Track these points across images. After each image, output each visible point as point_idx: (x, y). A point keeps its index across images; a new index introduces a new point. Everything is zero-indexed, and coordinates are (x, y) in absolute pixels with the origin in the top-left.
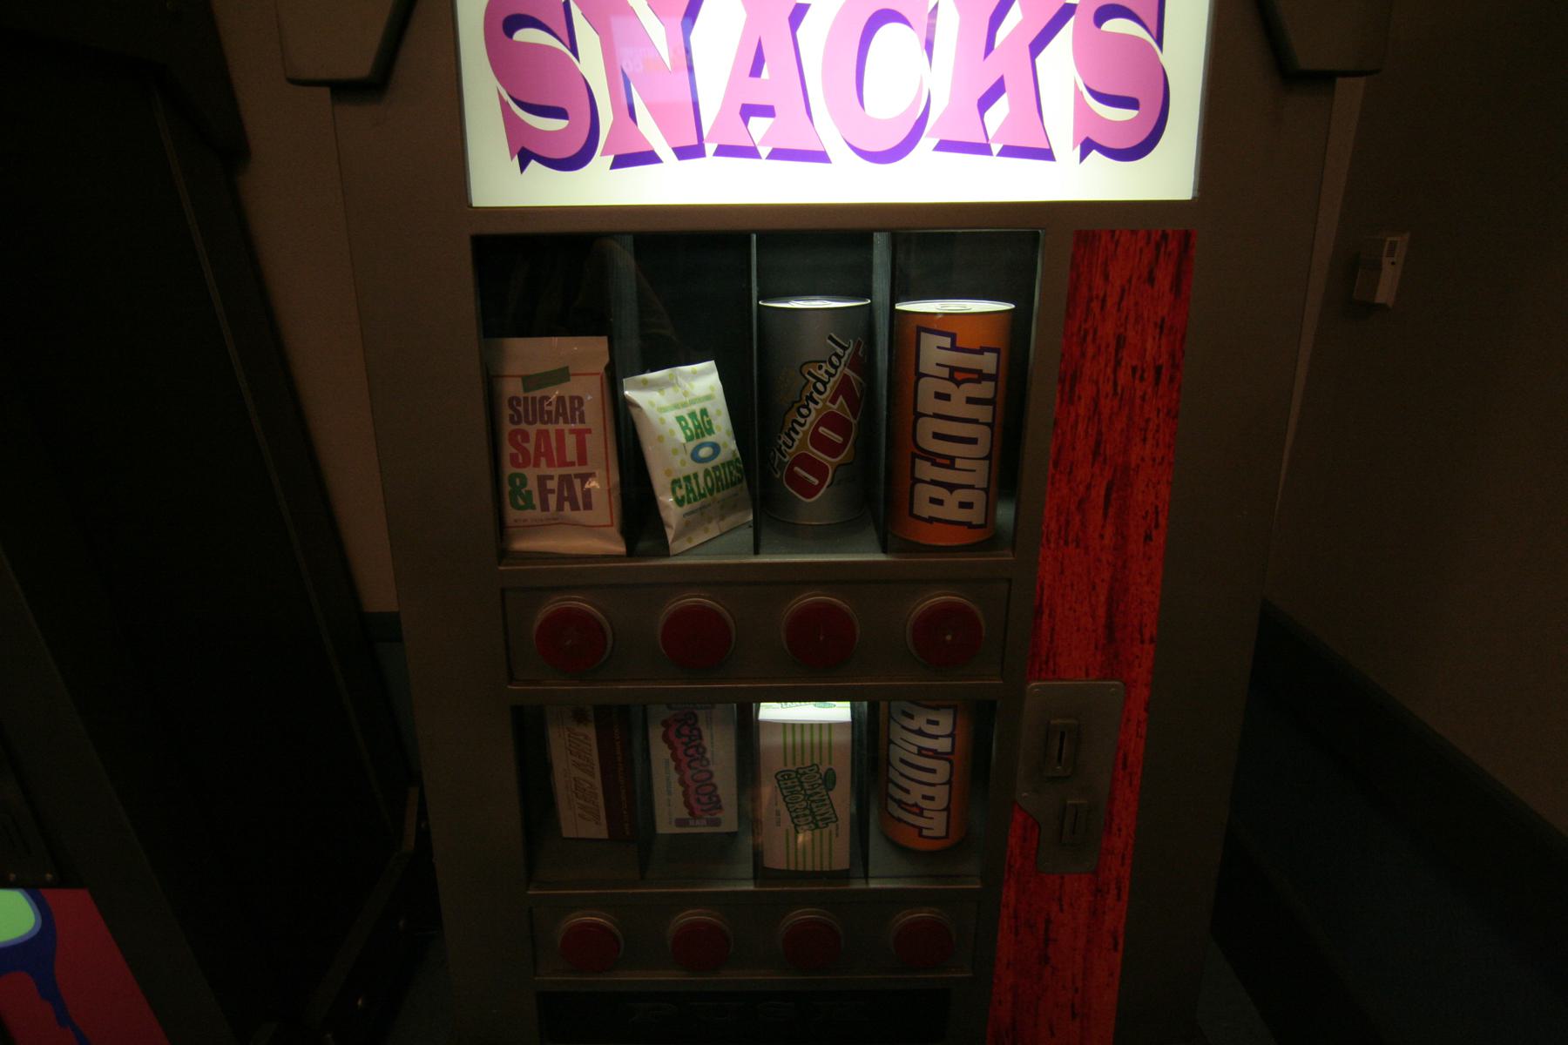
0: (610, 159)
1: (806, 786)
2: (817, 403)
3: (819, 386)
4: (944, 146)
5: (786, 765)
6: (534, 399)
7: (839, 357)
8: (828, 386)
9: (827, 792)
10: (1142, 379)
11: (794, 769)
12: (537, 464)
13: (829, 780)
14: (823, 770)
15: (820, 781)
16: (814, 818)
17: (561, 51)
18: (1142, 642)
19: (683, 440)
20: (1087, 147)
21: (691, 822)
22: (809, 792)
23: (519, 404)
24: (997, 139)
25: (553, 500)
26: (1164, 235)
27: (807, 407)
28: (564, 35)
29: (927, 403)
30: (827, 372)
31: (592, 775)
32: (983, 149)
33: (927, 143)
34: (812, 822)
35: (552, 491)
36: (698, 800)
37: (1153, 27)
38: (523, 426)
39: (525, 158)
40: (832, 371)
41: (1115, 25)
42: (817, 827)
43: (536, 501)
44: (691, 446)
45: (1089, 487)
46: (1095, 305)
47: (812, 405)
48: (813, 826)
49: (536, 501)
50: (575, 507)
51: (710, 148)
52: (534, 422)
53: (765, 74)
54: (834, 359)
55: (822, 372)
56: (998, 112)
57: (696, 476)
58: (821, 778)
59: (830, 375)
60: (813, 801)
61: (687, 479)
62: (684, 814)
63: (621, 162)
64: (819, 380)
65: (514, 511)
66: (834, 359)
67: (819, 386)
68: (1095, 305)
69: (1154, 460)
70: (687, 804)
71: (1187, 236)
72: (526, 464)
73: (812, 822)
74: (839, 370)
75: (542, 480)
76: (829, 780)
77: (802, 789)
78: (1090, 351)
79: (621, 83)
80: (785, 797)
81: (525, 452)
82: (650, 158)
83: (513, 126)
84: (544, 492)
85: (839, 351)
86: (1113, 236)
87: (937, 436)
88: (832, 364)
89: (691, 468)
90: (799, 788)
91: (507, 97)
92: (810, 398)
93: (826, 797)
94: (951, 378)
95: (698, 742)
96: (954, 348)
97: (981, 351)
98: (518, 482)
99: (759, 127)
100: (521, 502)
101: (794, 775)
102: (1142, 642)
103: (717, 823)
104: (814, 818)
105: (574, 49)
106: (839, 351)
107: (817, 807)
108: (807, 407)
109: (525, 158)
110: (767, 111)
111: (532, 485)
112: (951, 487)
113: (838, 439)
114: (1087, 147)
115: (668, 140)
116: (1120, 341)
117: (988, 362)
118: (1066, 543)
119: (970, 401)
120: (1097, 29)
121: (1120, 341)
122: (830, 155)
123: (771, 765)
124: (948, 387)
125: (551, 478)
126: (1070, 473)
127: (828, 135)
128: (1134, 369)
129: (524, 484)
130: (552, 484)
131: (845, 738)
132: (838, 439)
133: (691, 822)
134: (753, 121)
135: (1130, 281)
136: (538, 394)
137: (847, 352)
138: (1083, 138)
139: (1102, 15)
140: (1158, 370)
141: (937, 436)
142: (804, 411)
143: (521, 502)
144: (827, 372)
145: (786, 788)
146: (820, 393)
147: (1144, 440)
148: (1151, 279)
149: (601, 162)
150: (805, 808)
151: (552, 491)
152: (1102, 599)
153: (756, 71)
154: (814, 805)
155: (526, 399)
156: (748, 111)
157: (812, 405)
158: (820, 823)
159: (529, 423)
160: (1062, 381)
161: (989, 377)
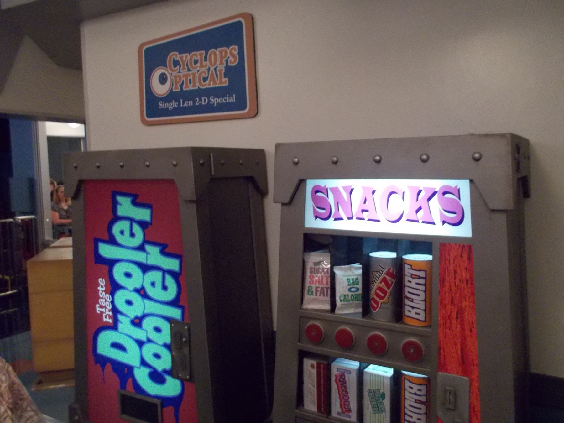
0: (333, 219)
1: (376, 396)
2: (376, 283)
3: (377, 278)
4: (408, 220)
5: (370, 387)
6: (316, 268)
7: (382, 271)
8: (380, 279)
9: (382, 400)
10: (463, 283)
11: (373, 389)
12: (316, 284)
13: (383, 396)
14: (381, 391)
15: (380, 396)
16: (378, 408)
17: (325, 197)
18: (446, 328)
19: (347, 285)
20: (444, 222)
21: (342, 414)
22: (377, 399)
23: (312, 269)
24: (421, 219)
25: (318, 293)
26: (464, 246)
27: (374, 284)
28: (326, 194)
29: (407, 284)
30: (379, 275)
31: (315, 388)
32: (418, 221)
33: (404, 219)
34: (378, 410)
35: (319, 291)
36: (344, 407)
37: (458, 196)
38: (313, 274)
39: (316, 217)
40: (380, 275)
41: (447, 196)
42: (379, 412)
43: (314, 293)
44: (349, 287)
45: (451, 312)
46: (447, 262)
47: (375, 283)
48: (378, 412)
49: (314, 293)
50: (324, 296)
51: (354, 218)
52: (316, 273)
53: (367, 202)
54: (381, 272)
55: (378, 274)
56: (421, 213)
57: (348, 295)
58: (380, 394)
59: (380, 276)
60: (378, 403)
61: (345, 296)
62: (340, 410)
63: (336, 219)
64: (377, 277)
65: (307, 295)
66: (381, 272)
67: (377, 278)
68: (447, 262)
69: (469, 307)
70: (341, 407)
71: (470, 247)
72: (312, 284)
73: (378, 410)
74: (382, 275)
75: (317, 288)
76: (383, 396)
77: (375, 397)
78: (447, 273)
79: (337, 204)
80: (370, 399)
81: (313, 281)
82: (341, 219)
83: (315, 211)
84: (317, 291)
85: (383, 270)
86: (450, 245)
87: (409, 292)
88: (380, 273)
89: (347, 292)
90: (374, 397)
91: (314, 205)
92: (375, 281)
93: (382, 402)
94: (411, 277)
95: (344, 385)
96: (411, 269)
97: (419, 270)
98: (310, 288)
99: (365, 214)
100: (310, 293)
101: (372, 392)
102: (474, 365)
103: (350, 417)
104: (378, 408)
105: (328, 197)
106: (383, 270)
107: (380, 405)
108: (374, 284)
109: (316, 217)
110: (367, 211)
111: (314, 289)
112: (413, 308)
113: (382, 295)
114: (444, 222)
115: (346, 216)
116: (455, 272)
117: (422, 274)
118: (446, 328)
119: (417, 284)
120: (443, 196)
121: (455, 272)
122: (381, 221)
123: (367, 387)
124: (411, 279)
125: (319, 287)
126: (445, 307)
127: (379, 215)
128: (460, 280)
129: (312, 288)
130: (319, 289)
131: (388, 383)
132: (382, 295)
133: (342, 414)
134: (364, 212)
135: (456, 256)
136: (317, 267)
137: (385, 270)
138: (442, 220)
139: (444, 193)
140: (467, 281)
141: (409, 292)
142: (373, 285)
143: (310, 293)
144: (379, 275)
145: (371, 396)
146: (377, 280)
147: (466, 300)
148: (462, 256)
149: (332, 219)
150: (376, 405)
151: (319, 291)
152: (459, 348)
153: (365, 203)
154: (378, 404)
155: (314, 268)
156: (363, 211)
157: (375, 283)
158: (380, 412)
159: (314, 273)
160: (440, 281)
161: (422, 278)
